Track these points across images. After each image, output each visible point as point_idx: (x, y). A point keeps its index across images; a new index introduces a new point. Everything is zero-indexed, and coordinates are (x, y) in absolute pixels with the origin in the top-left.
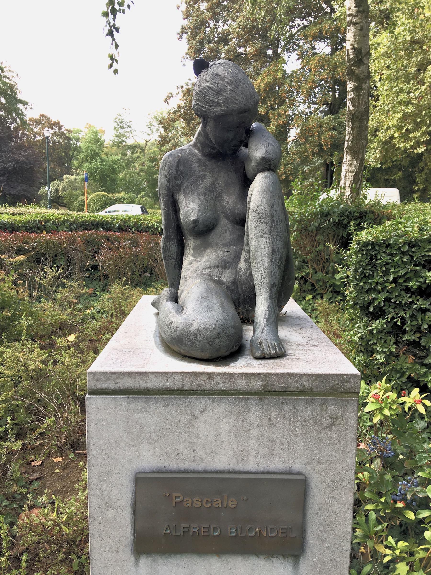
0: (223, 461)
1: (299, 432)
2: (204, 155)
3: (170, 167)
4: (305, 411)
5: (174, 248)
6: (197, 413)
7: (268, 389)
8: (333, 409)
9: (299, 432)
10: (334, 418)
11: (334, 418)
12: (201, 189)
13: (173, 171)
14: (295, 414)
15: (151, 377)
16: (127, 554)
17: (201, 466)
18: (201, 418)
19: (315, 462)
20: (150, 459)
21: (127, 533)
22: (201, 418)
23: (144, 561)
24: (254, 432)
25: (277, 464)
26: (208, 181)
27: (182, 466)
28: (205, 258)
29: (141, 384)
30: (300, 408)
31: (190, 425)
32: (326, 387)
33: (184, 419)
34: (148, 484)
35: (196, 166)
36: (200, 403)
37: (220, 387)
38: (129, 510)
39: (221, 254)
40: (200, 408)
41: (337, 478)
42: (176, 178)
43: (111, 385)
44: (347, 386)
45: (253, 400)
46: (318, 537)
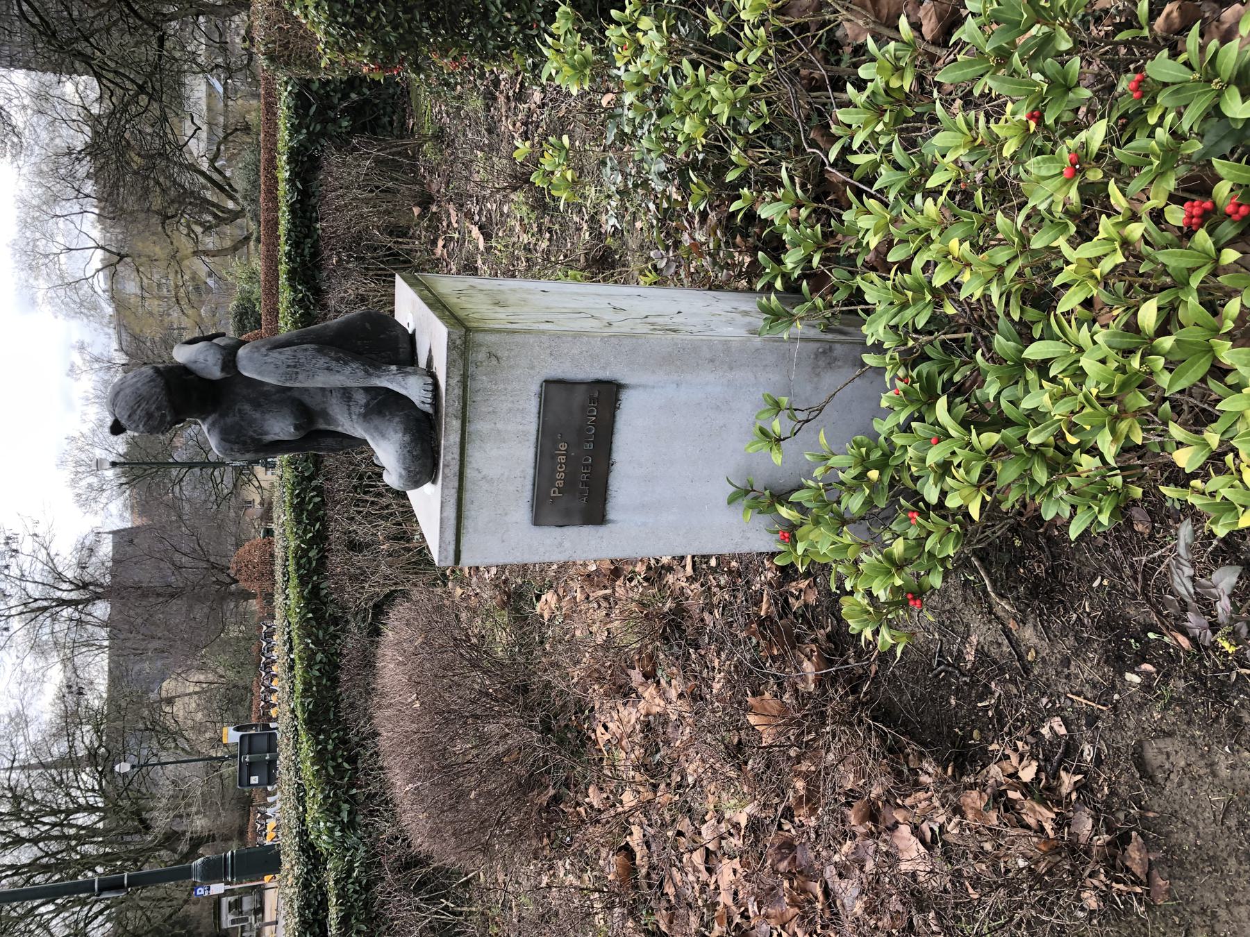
0: (527, 453)
1: (502, 386)
2: (214, 411)
3: (232, 450)
4: (482, 380)
5: (330, 441)
6: (480, 476)
7: (460, 415)
8: (481, 356)
9: (502, 386)
10: (490, 355)
11: (490, 355)
12: (257, 415)
13: (236, 447)
14: (485, 390)
15: (445, 514)
16: (602, 530)
17: (531, 472)
18: (485, 472)
19: (532, 372)
20: (522, 512)
21: (587, 531)
22: (485, 472)
23: (611, 515)
24: (500, 426)
25: (532, 406)
26: (247, 407)
27: (529, 486)
28: (339, 417)
29: (452, 522)
30: (479, 385)
31: (491, 481)
32: (460, 363)
33: (485, 486)
34: (547, 509)
35: (229, 420)
36: (470, 473)
37: (457, 457)
38: (565, 529)
39: (334, 401)
40: (475, 474)
41: (548, 351)
42: (244, 443)
43: (452, 548)
44: (458, 342)
45: (470, 428)
46: (604, 368)
